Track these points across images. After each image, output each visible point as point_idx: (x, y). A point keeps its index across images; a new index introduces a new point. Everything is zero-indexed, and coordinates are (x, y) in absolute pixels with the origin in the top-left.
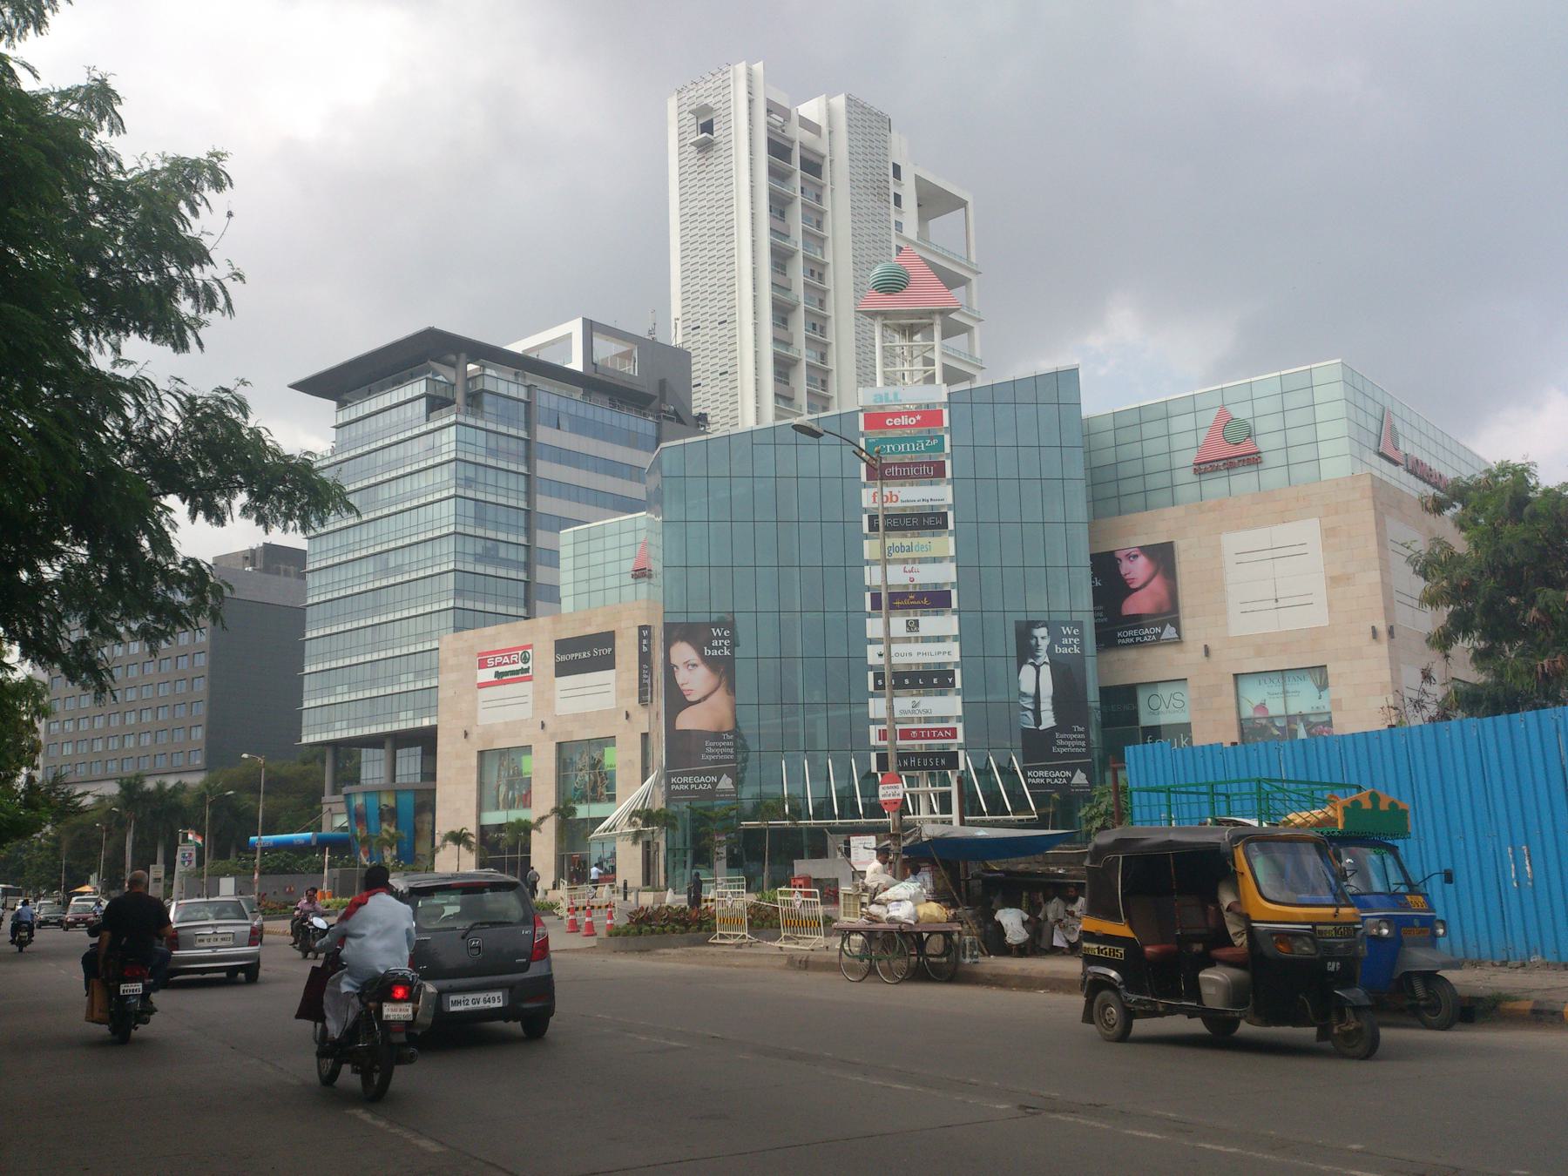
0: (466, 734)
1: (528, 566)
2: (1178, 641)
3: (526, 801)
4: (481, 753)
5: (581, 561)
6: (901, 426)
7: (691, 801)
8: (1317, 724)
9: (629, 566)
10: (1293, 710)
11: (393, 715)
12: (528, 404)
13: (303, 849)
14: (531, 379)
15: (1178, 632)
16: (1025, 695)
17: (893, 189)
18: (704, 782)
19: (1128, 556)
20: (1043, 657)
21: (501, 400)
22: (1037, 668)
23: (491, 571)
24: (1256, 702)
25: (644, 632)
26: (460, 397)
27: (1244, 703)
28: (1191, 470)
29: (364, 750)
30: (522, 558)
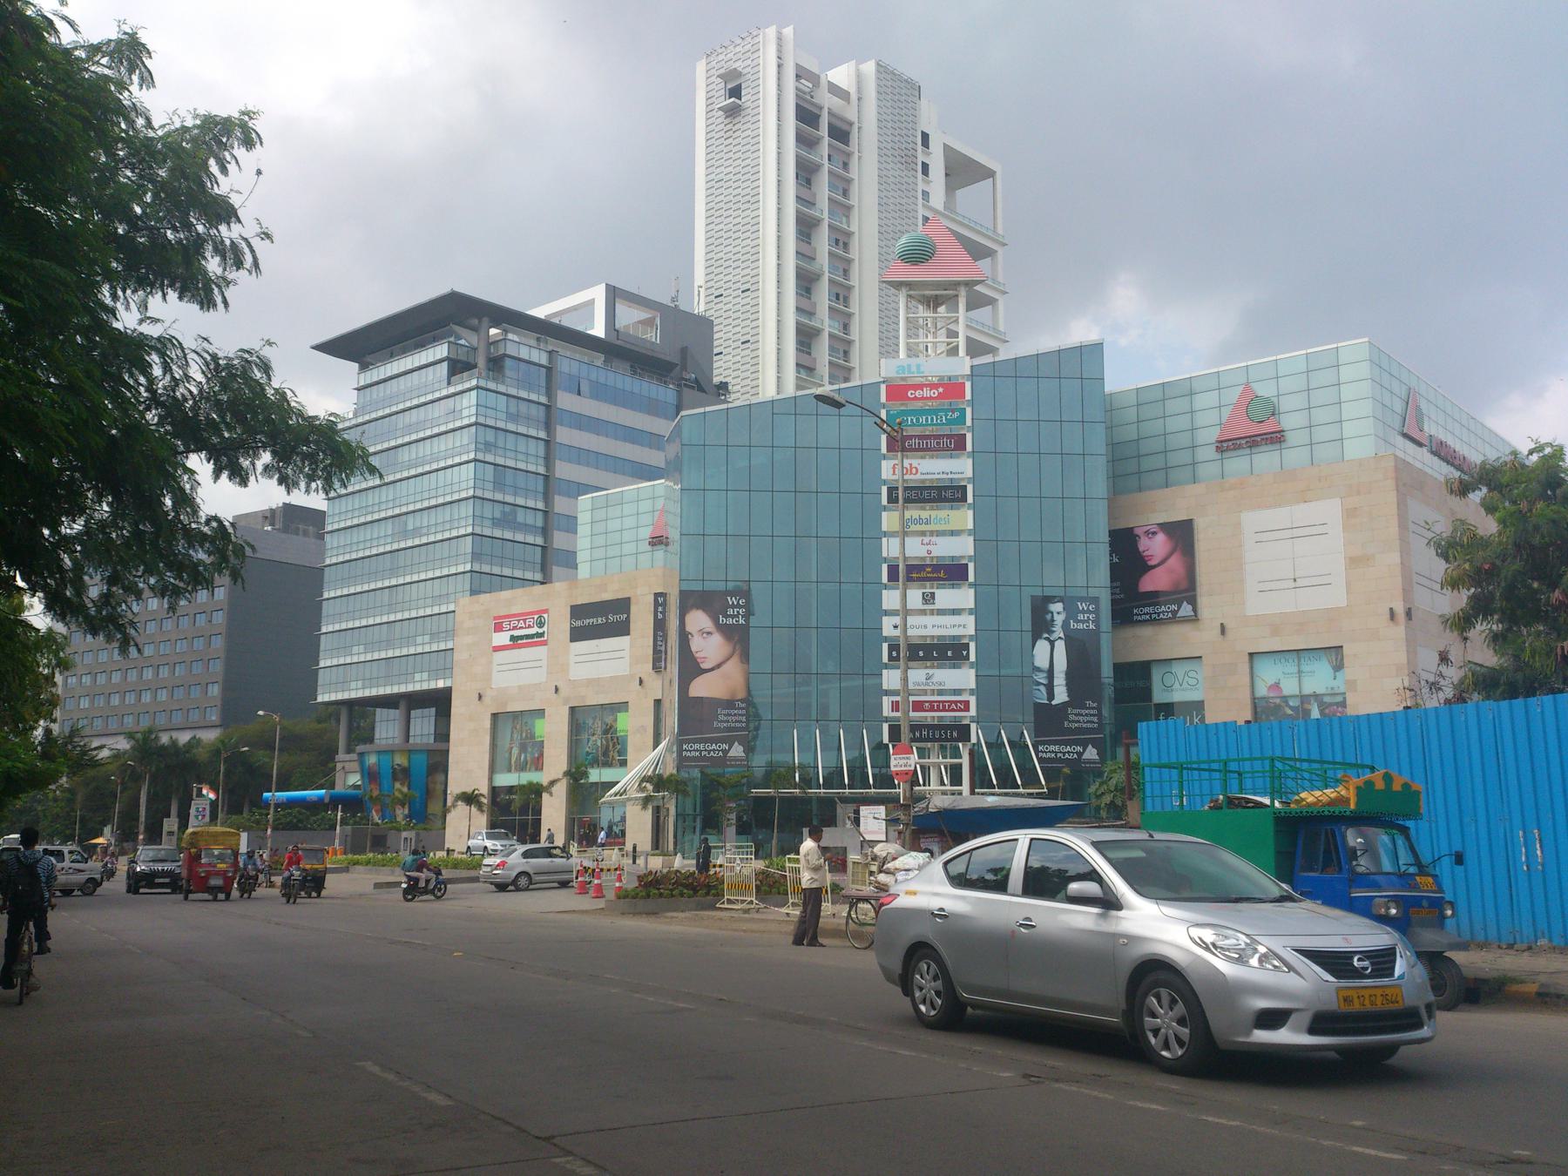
0: (480, 697)
1: (545, 531)
2: (1195, 618)
3: (538, 764)
4: (495, 716)
5: (600, 528)
6: (923, 398)
8: (1331, 704)
9: (646, 533)
10: (1307, 690)
11: (407, 676)
13: (315, 806)
14: (553, 344)
15: (1195, 610)
16: (1039, 670)
17: (921, 158)
19: (1147, 533)
20: (1058, 632)
21: (522, 365)
22: (1052, 643)
23: (508, 535)
24: (1271, 682)
25: (660, 600)
26: (481, 362)
29: (378, 711)
30: (540, 523)
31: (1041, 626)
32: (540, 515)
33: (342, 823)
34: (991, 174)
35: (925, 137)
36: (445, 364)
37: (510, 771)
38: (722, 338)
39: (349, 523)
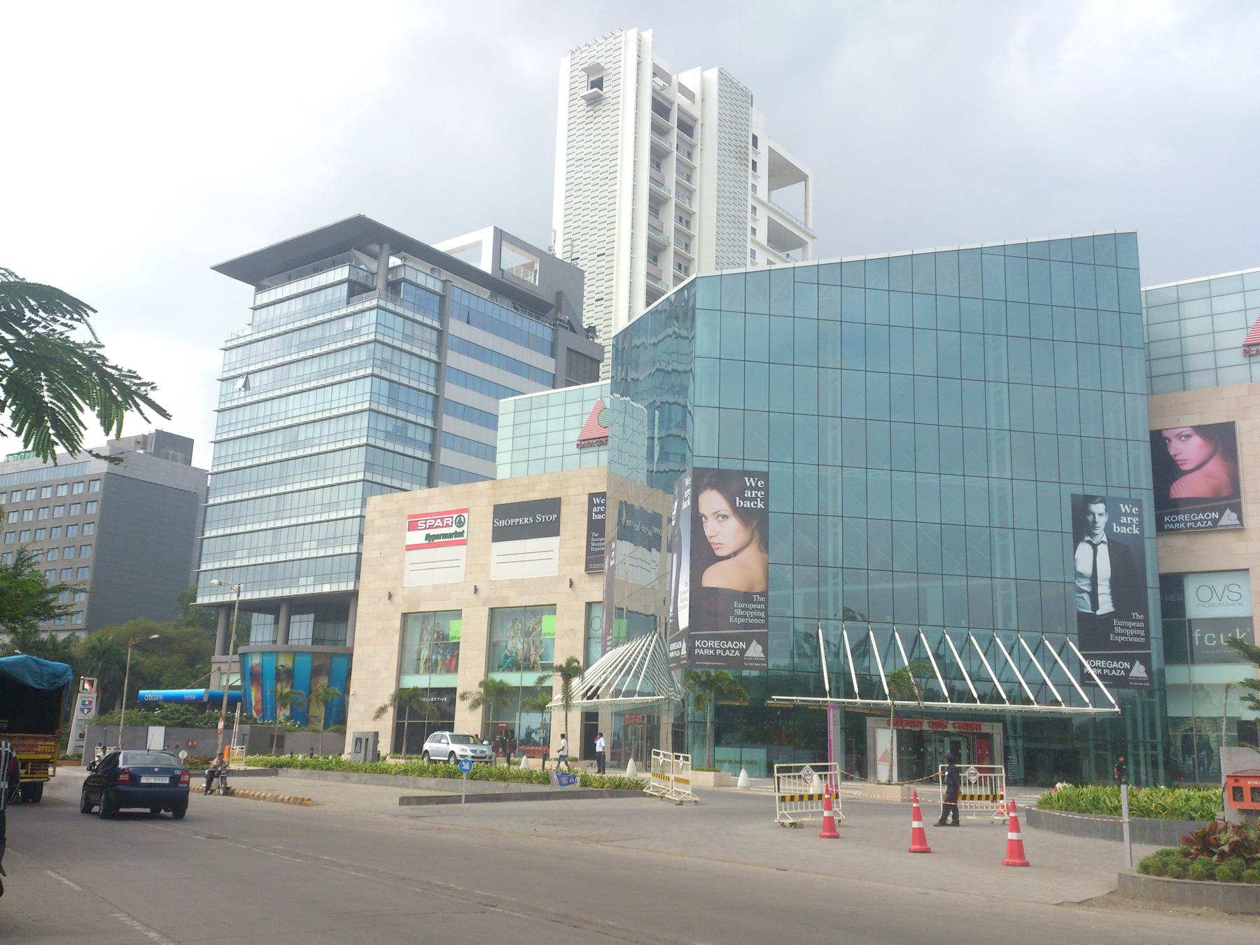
0: (390, 596)
1: (433, 448)
2: (1239, 528)
4: (405, 615)
5: (523, 430)
11: (293, 580)
13: (198, 703)
14: (446, 275)
15: (1240, 518)
16: (1081, 575)
18: (732, 648)
19: (1179, 436)
20: (1101, 535)
21: (420, 292)
22: (1095, 547)
23: (399, 448)
25: (595, 500)
26: (380, 284)
28: (1240, 352)
29: (255, 615)
30: (428, 439)
31: (1082, 529)
32: (428, 432)
33: (241, 722)
34: (804, 178)
35: (755, 138)
36: (345, 286)
37: (417, 672)
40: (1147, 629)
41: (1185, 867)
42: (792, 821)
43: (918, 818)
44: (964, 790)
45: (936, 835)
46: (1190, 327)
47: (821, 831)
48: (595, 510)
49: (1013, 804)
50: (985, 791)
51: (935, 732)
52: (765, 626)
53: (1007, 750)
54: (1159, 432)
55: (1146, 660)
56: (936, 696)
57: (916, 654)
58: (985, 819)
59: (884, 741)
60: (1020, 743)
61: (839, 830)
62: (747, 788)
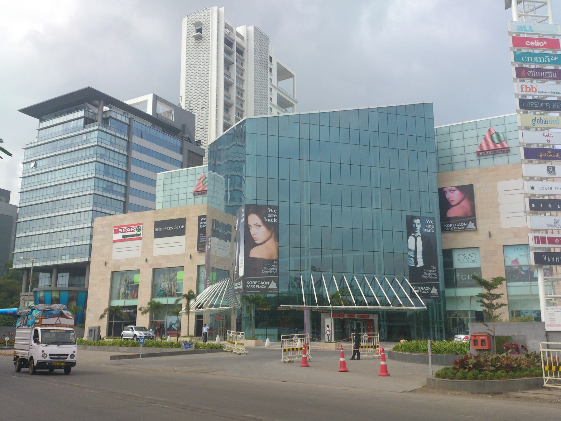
0: (106, 264)
1: (126, 195)
2: (475, 230)
3: (135, 296)
4: (113, 273)
5: (168, 187)
6: (535, 47)
7: (256, 293)
9: (192, 190)
11: (59, 257)
12: (129, 126)
14: (130, 115)
15: (475, 225)
16: (410, 250)
17: (269, 66)
18: (262, 285)
19: (450, 190)
20: (418, 233)
21: (118, 123)
22: (416, 238)
23: (109, 195)
24: (513, 259)
25: (201, 219)
26: (99, 119)
27: (507, 259)
28: (476, 154)
29: (41, 273)
30: (123, 191)
31: (411, 230)
32: (123, 188)
34: (292, 76)
35: (271, 58)
36: (82, 120)
38: (198, 124)
39: (32, 188)
40: (437, 273)
41: (454, 374)
42: (288, 360)
43: (343, 356)
44: (362, 344)
45: (350, 364)
46: (455, 144)
47: (301, 364)
48: (201, 223)
49: (383, 349)
50: (371, 344)
51: (350, 319)
52: (277, 274)
53: (380, 326)
54: (442, 189)
55: (437, 287)
56: (351, 304)
57: (342, 286)
58: (371, 356)
59: (328, 323)
60: (385, 323)
61: (309, 363)
62: (269, 346)
